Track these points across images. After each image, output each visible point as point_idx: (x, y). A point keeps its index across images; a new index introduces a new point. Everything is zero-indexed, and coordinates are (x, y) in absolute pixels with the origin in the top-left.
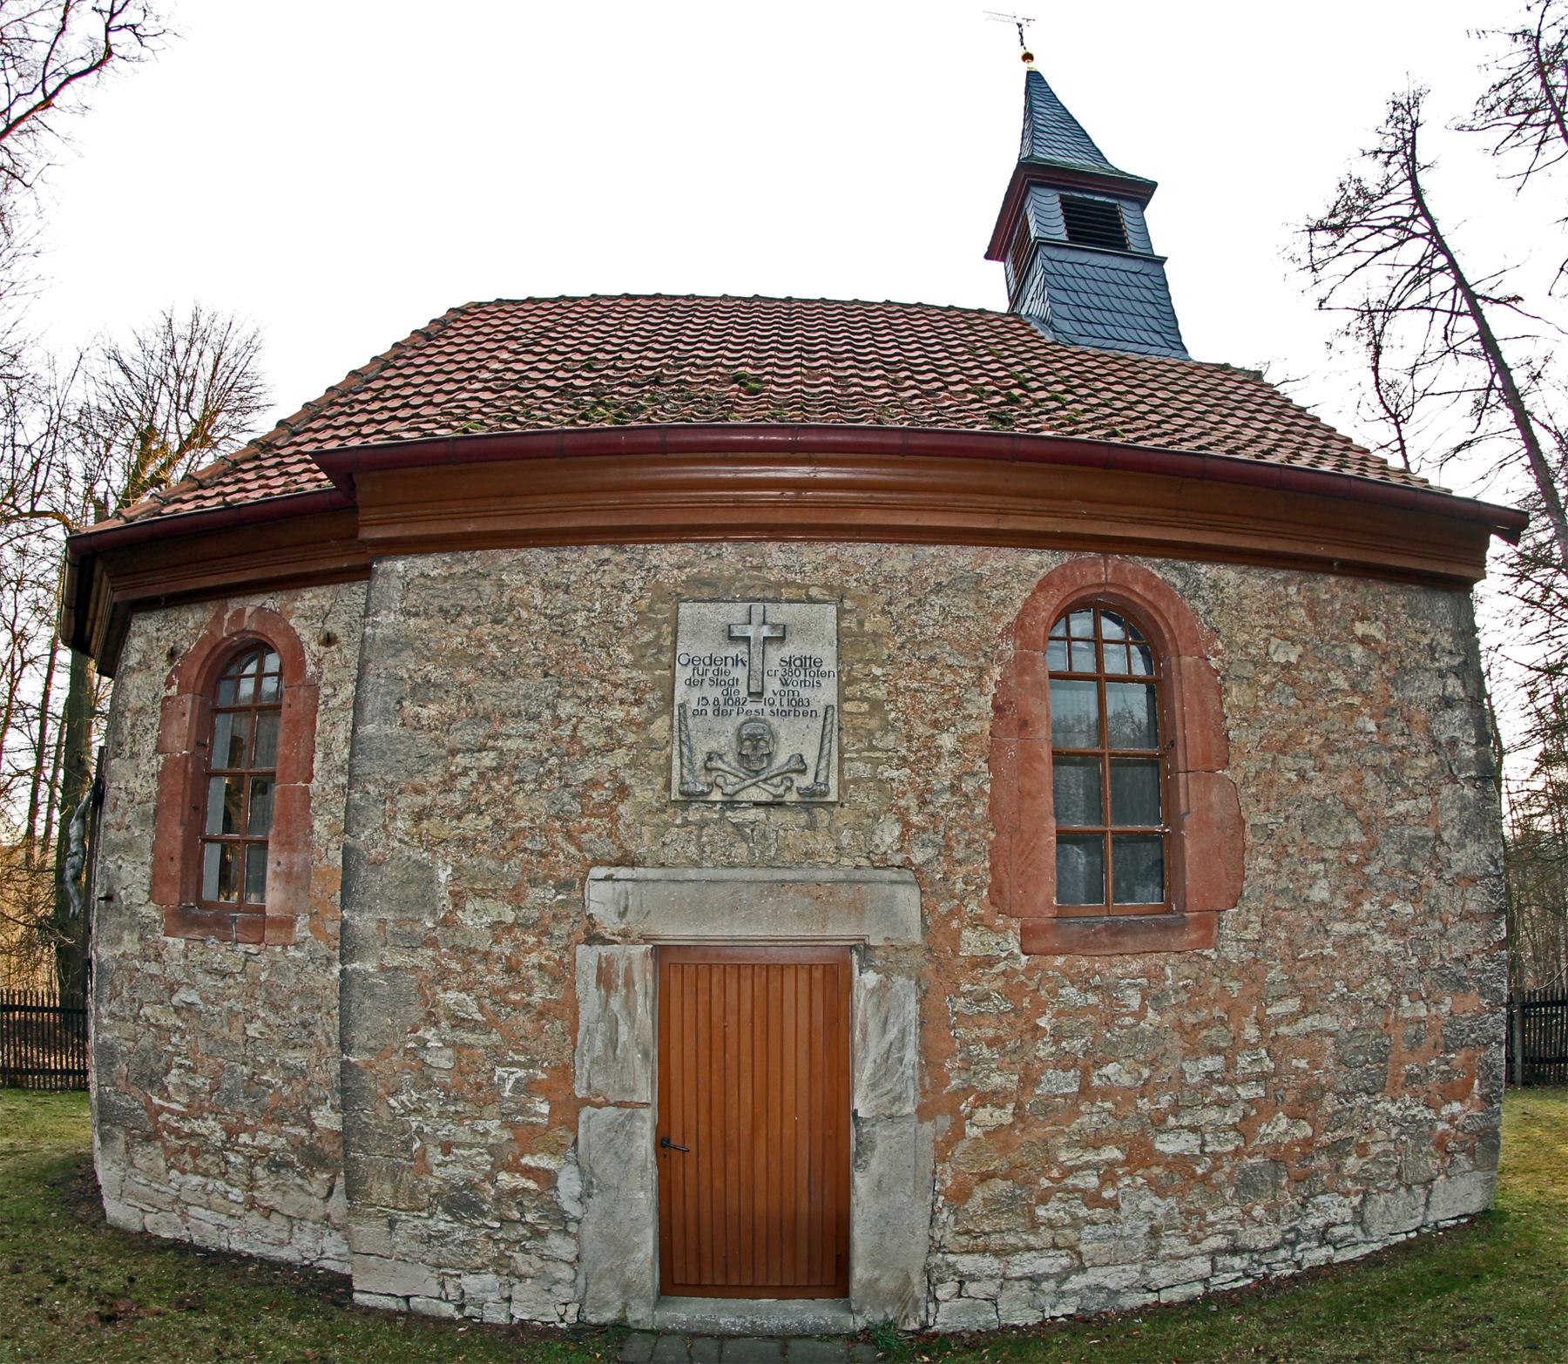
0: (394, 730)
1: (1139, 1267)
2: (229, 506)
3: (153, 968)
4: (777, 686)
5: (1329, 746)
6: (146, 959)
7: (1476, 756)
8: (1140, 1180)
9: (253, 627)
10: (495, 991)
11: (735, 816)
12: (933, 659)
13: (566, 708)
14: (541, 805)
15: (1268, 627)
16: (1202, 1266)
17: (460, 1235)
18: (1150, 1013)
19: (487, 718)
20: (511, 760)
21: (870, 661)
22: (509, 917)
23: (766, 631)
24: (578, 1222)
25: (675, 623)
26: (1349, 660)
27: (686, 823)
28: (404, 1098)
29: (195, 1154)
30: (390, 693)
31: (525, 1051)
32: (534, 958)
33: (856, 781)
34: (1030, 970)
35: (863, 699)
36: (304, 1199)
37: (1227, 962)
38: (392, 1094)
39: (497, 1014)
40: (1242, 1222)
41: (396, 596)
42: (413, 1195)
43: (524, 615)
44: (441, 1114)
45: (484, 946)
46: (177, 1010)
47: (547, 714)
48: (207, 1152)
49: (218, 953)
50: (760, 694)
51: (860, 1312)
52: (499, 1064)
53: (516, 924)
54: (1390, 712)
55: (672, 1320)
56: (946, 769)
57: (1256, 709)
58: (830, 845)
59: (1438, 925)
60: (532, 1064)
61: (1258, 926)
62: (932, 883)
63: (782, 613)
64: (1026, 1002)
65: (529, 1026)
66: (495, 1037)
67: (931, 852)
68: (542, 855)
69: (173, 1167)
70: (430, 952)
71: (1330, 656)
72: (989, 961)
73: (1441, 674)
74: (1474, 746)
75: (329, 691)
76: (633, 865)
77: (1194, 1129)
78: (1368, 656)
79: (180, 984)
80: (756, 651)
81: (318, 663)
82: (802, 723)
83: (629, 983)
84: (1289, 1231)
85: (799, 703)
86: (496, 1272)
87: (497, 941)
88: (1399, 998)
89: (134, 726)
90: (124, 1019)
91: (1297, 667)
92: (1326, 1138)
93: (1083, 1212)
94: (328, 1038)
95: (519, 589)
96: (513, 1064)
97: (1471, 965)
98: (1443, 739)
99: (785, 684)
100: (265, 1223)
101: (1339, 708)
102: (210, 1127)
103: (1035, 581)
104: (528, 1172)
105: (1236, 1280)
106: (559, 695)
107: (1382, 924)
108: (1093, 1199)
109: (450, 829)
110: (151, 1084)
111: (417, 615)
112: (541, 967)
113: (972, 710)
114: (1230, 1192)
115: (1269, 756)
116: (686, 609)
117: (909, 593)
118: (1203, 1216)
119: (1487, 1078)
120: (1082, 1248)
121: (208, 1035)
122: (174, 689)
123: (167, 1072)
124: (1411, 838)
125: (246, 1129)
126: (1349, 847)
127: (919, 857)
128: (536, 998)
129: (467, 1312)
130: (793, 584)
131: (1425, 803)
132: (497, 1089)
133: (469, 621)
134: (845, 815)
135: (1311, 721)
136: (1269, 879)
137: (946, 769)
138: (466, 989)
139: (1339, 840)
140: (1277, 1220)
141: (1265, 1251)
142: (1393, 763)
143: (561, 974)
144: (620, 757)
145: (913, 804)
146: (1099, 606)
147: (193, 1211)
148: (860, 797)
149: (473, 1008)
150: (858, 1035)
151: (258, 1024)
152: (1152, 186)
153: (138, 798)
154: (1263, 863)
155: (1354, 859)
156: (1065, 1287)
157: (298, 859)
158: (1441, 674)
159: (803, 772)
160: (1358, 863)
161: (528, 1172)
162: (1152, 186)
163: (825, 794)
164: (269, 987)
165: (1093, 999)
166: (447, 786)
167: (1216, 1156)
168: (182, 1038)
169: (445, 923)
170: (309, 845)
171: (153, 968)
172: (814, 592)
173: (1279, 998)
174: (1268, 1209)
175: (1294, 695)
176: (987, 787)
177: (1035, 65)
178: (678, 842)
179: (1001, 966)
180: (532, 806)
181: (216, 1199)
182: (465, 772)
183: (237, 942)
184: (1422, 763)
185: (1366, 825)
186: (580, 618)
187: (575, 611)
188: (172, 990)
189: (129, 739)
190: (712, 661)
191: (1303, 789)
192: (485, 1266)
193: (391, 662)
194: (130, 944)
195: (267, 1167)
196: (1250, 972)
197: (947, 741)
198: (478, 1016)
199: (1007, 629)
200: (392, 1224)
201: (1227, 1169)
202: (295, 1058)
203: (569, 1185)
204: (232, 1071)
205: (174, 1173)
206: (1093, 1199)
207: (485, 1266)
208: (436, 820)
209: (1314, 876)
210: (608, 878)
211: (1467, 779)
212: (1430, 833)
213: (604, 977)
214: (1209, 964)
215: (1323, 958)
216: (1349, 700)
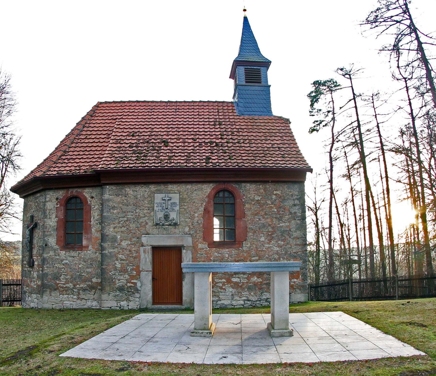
0: (109, 214)
1: (230, 301)
2: (73, 175)
3: (58, 257)
4: (170, 207)
5: (266, 214)
6: (56, 256)
7: (301, 215)
8: (229, 286)
9: (76, 194)
10: (127, 254)
11: (164, 227)
12: (194, 202)
13: (137, 211)
14: (134, 225)
15: (255, 193)
16: (242, 302)
17: (121, 295)
18: (230, 258)
19: (125, 212)
20: (129, 219)
21: (184, 203)
22: (130, 243)
23: (168, 198)
24: (140, 291)
25: (154, 197)
26: (272, 199)
27: (156, 228)
28: (112, 272)
29: (66, 291)
30: (108, 208)
31: (132, 264)
32: (134, 249)
33: (182, 221)
34: (209, 250)
35: (183, 209)
36: (89, 295)
37: (244, 250)
38: (110, 272)
39: (128, 258)
40: (249, 295)
41: (108, 192)
42: (113, 289)
43: (130, 196)
44: (118, 275)
45: (125, 248)
46: (63, 264)
47: (135, 212)
48: (69, 290)
49: (73, 253)
50: (167, 208)
51: (184, 305)
52: (128, 266)
53: (131, 244)
54: (280, 208)
55: (154, 307)
56: (196, 219)
57: (251, 208)
58: (178, 231)
59: (289, 246)
60: (133, 265)
61: (250, 245)
62: (194, 236)
63: (171, 195)
64: (209, 255)
65: (133, 260)
66: (127, 262)
67: (194, 232)
68: (135, 233)
69: (61, 294)
70: (117, 249)
71: (268, 198)
72: (203, 249)
73: (294, 200)
74: (301, 213)
75: (93, 207)
76: (149, 234)
77: (239, 278)
78: (276, 197)
79: (64, 260)
80: (167, 202)
81: (91, 201)
82: (174, 213)
83: (148, 252)
84: (259, 298)
85: (173, 209)
86: (127, 301)
87: (128, 247)
88: (280, 258)
89: (49, 212)
90: (50, 268)
91: (260, 200)
92: (265, 282)
93: (220, 290)
94: (96, 266)
95: (129, 191)
96: (130, 266)
97: (298, 254)
98: (293, 212)
99: (171, 206)
100: (81, 301)
101: (268, 207)
102: (71, 285)
103: (212, 188)
104: (132, 283)
105: (249, 306)
106: (136, 209)
107: (276, 245)
108: (221, 288)
109: (120, 230)
110: (57, 279)
111: (111, 195)
112: (135, 250)
113: (200, 210)
114: (246, 289)
115: (253, 216)
116: (156, 195)
117: (191, 191)
118: (241, 293)
119: (303, 275)
120: (220, 296)
121: (70, 268)
122: (59, 205)
123: (61, 276)
124: (283, 230)
125: (78, 284)
126: (269, 232)
127: (192, 233)
128: (134, 255)
129: (121, 308)
130: (172, 190)
131: (287, 224)
132: (127, 270)
133: (121, 197)
134: (180, 226)
135: (262, 210)
136: (252, 237)
137: (196, 219)
138: (123, 255)
139: (267, 230)
140: (256, 296)
141: (254, 301)
142: (280, 217)
143: (138, 252)
144: (146, 218)
145: (191, 225)
146: (224, 190)
147: (65, 302)
148: (183, 224)
149: (124, 257)
150: (183, 260)
151: (81, 265)
152: (271, 62)
153: (52, 226)
154: (251, 234)
155: (270, 233)
156: (217, 303)
157: (89, 236)
158: (294, 200)
159: (174, 220)
160: (271, 234)
161: (132, 283)
162: (271, 62)
163: (177, 223)
164: (84, 258)
165: (220, 255)
166: (119, 223)
167: (243, 283)
168: (64, 269)
169: (119, 244)
170: (91, 233)
171: (58, 257)
172: (176, 191)
173: (254, 257)
174: (254, 293)
175: (259, 205)
176: (202, 222)
177: (247, 14)
178: (155, 231)
179: (205, 249)
180: (133, 226)
181: (70, 299)
182: (122, 221)
183: (77, 251)
184: (287, 217)
185: (273, 228)
186: (139, 196)
187: (138, 195)
188: (62, 261)
189: (49, 215)
190: (160, 203)
191: (260, 222)
192: (125, 300)
193: (108, 203)
194: (52, 253)
195: (83, 291)
196: (248, 252)
197: (196, 215)
198: (125, 259)
199: (206, 197)
200: (109, 294)
201: (245, 285)
202: (89, 270)
203: (139, 284)
204: (76, 274)
205: (61, 295)
206: (221, 288)
207: (125, 300)
208: (117, 228)
209: (261, 236)
210: (145, 237)
211: (298, 220)
212: (288, 229)
213: (144, 252)
214: (240, 250)
215: (263, 250)
216: (271, 206)
